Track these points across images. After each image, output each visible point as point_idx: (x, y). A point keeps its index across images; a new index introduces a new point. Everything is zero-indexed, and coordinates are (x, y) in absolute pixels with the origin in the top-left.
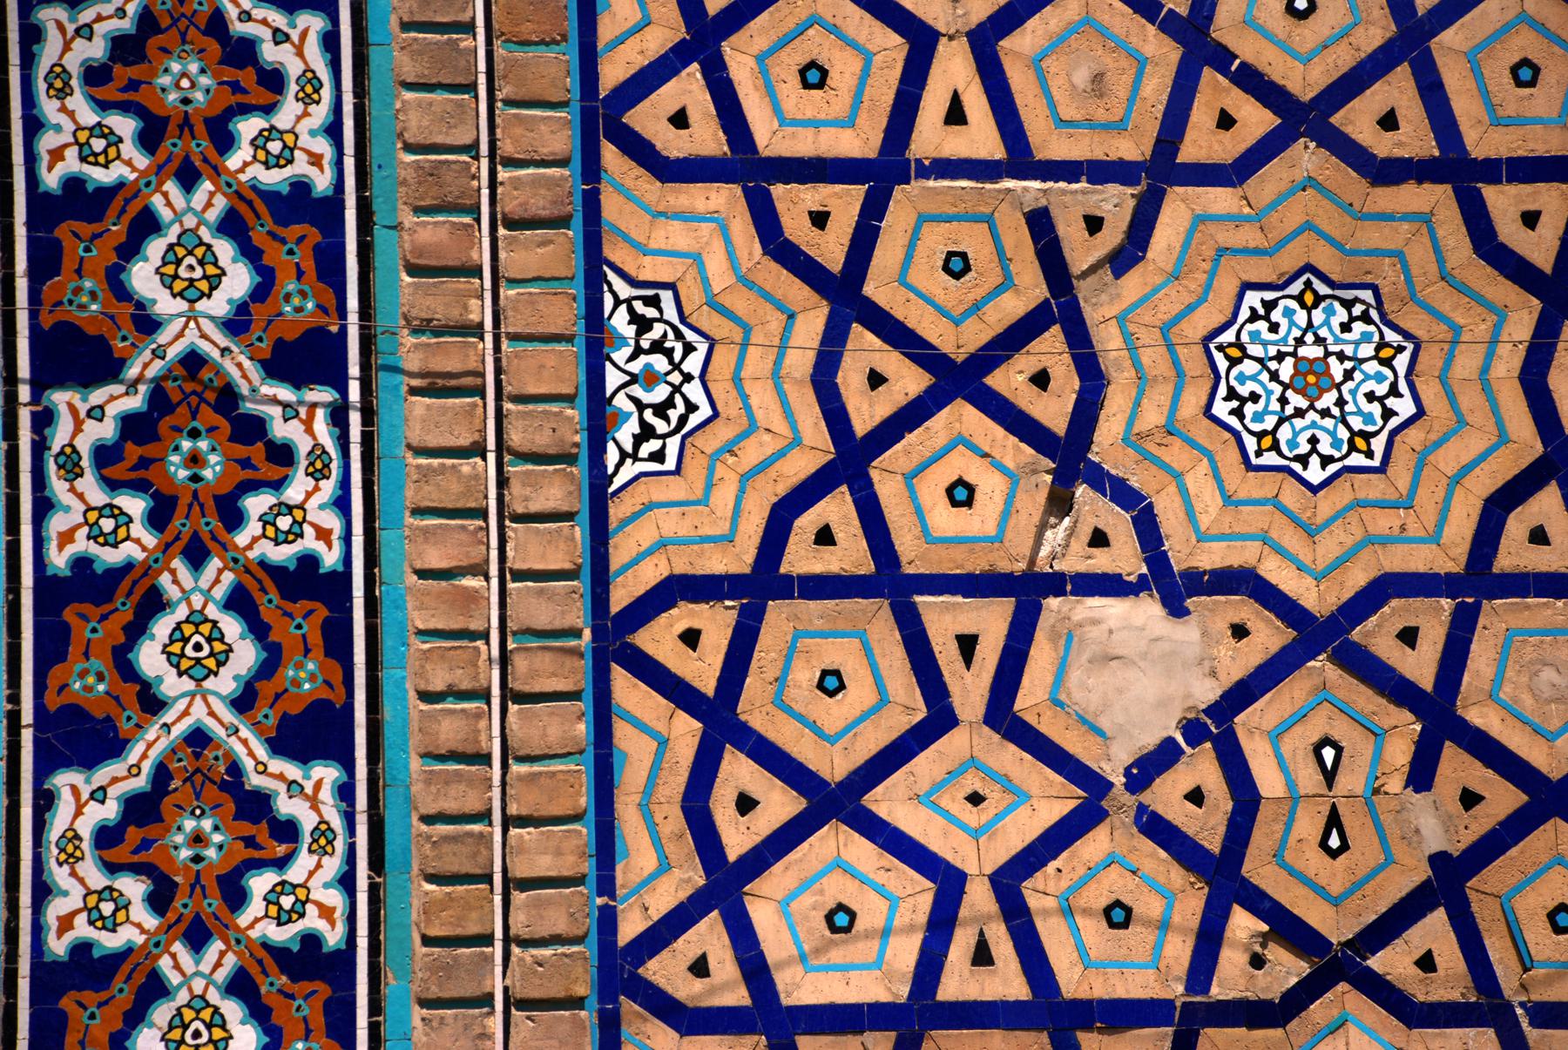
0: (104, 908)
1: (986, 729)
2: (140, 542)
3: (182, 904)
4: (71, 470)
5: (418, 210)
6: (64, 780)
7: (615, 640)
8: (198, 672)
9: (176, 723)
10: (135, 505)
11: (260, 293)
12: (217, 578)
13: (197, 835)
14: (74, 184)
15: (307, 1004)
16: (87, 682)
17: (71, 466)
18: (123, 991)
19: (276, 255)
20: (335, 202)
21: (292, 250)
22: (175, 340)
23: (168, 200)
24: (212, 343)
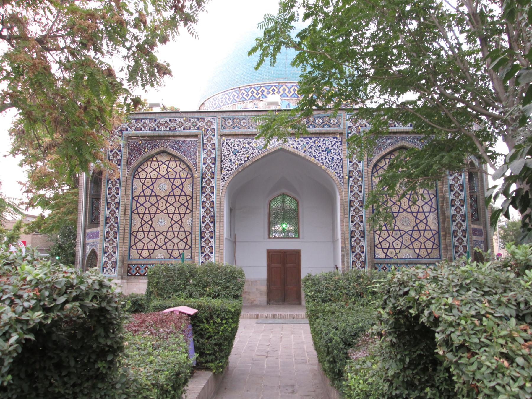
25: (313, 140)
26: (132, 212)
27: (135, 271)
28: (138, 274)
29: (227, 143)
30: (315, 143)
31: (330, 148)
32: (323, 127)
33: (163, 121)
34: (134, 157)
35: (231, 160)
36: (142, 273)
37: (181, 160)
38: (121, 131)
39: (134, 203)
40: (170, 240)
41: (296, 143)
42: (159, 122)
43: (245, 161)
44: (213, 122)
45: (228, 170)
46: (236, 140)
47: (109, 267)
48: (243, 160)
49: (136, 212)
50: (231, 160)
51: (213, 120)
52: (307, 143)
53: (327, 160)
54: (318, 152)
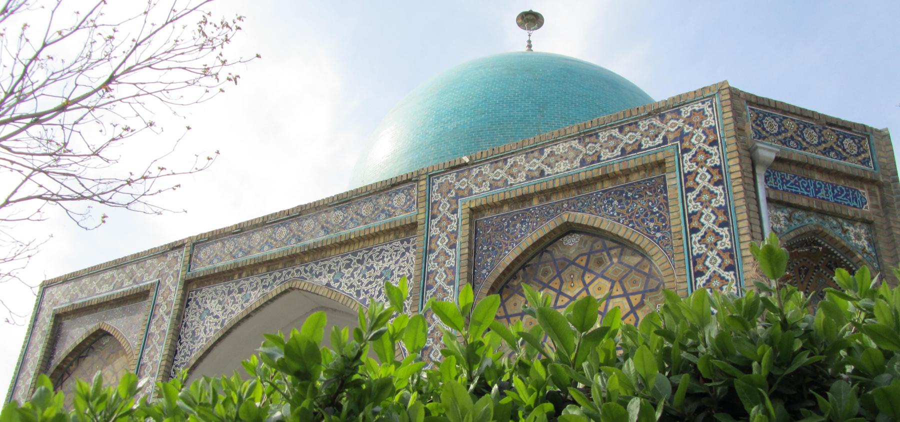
0: (700, 249)
1: (545, 416)
2: (695, 167)
3: (710, 247)
4: (695, 243)
5: (763, 239)
6: (698, 279)
8: (713, 264)
9: (701, 185)
10: (703, 246)
11: (722, 262)
12: (715, 252)
13: (701, 157)
14: (698, 254)
15: (717, 171)
16: (699, 267)
17: (695, 243)
18: (694, 175)
19: (724, 257)
20: (715, 127)
21: (720, 213)
22: (707, 226)
23: (700, 170)
24: (706, 184)
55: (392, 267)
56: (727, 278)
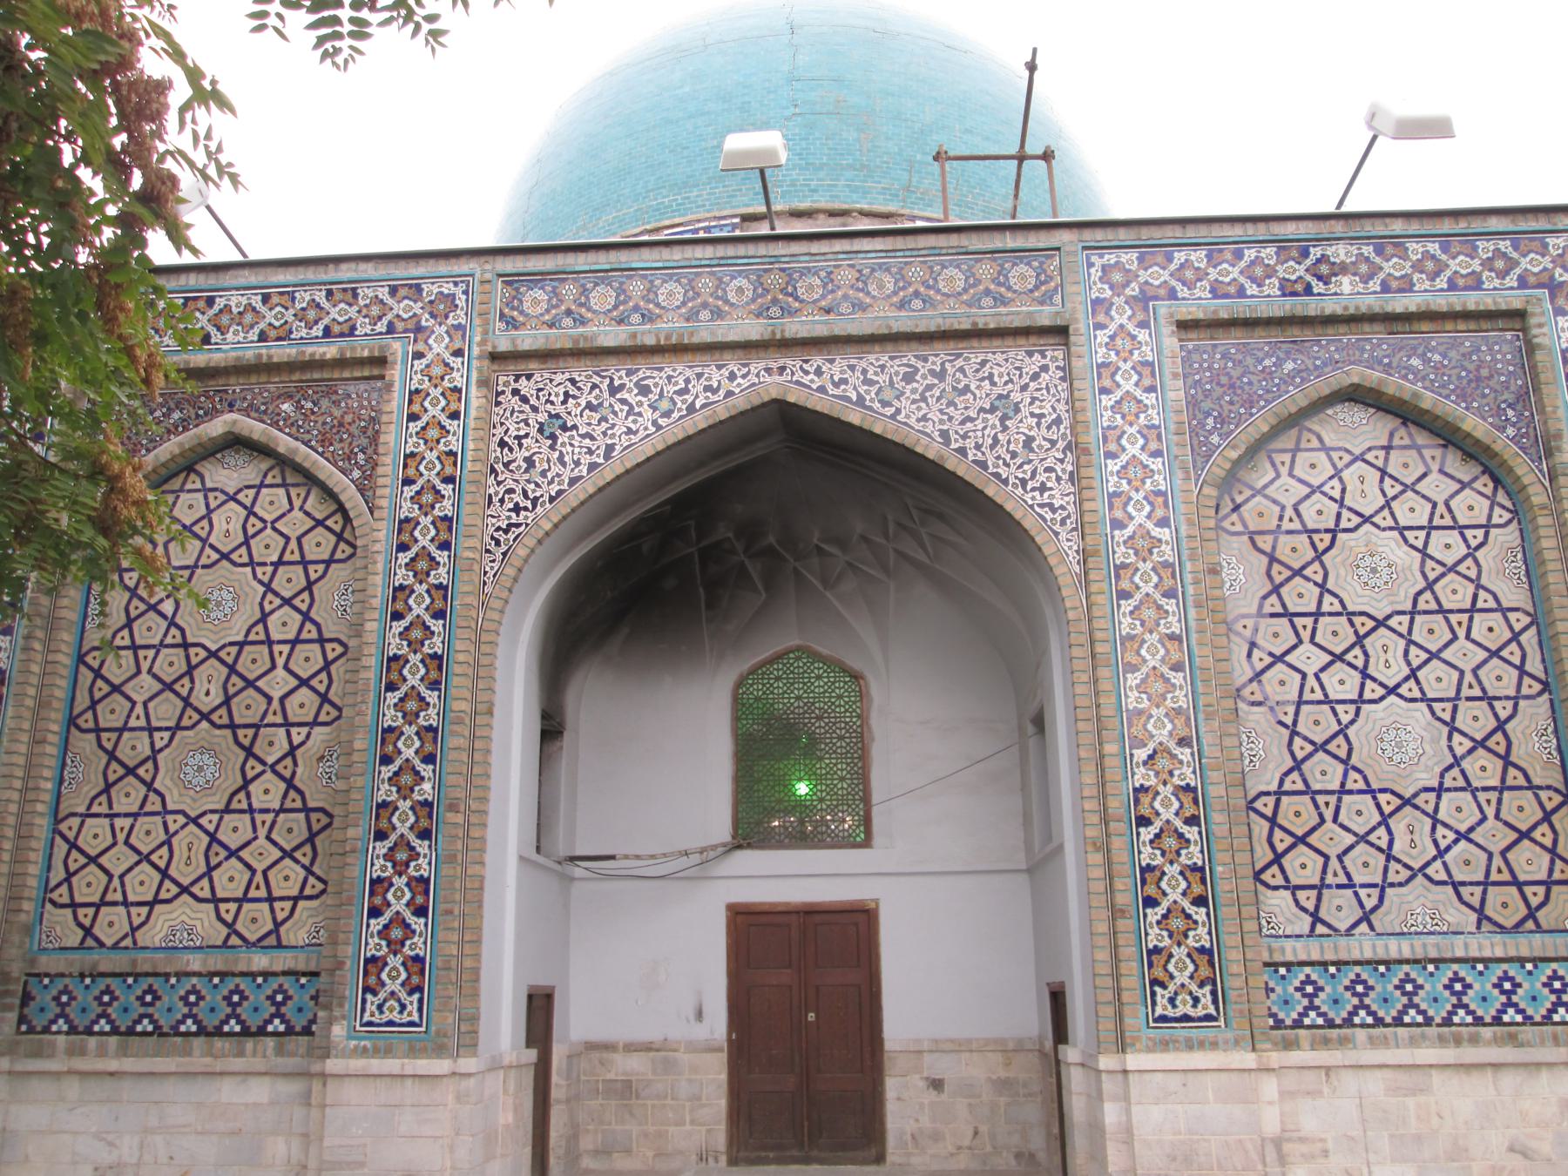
7: (81, 659)
25: (935, 363)
26: (72, 722)
27: (1449, 1001)
28: (103, 1025)
29: (516, 392)
30: (941, 375)
31: (1016, 396)
32: (902, 305)
33: (236, 301)
34: (1222, 420)
35: (530, 462)
36: (165, 1022)
37: (310, 479)
38: (419, 329)
39: (86, 676)
40: (93, 860)
41: (855, 378)
42: (227, 309)
43: (593, 467)
44: (461, 300)
45: (517, 509)
46: (559, 378)
47: (1182, 978)
48: (586, 459)
49: (87, 721)
50: (530, 462)
51: (458, 291)
52: (909, 378)
53: (1001, 451)
54: (958, 417)
55: (542, 417)
56: (1187, 836)
